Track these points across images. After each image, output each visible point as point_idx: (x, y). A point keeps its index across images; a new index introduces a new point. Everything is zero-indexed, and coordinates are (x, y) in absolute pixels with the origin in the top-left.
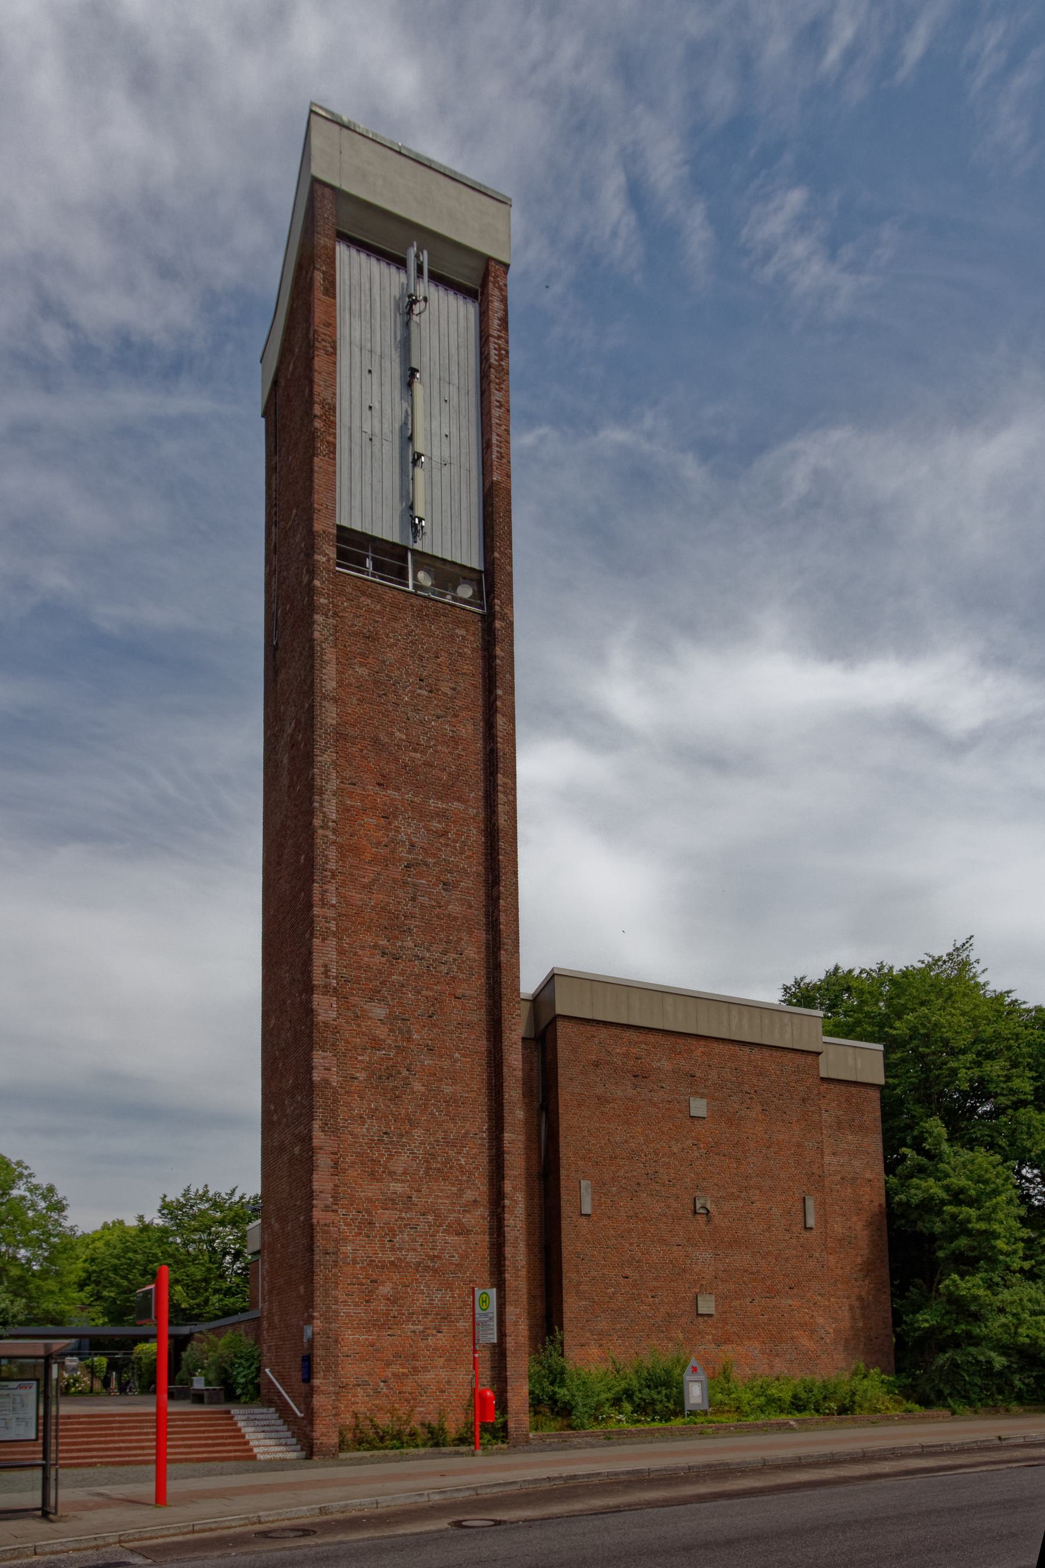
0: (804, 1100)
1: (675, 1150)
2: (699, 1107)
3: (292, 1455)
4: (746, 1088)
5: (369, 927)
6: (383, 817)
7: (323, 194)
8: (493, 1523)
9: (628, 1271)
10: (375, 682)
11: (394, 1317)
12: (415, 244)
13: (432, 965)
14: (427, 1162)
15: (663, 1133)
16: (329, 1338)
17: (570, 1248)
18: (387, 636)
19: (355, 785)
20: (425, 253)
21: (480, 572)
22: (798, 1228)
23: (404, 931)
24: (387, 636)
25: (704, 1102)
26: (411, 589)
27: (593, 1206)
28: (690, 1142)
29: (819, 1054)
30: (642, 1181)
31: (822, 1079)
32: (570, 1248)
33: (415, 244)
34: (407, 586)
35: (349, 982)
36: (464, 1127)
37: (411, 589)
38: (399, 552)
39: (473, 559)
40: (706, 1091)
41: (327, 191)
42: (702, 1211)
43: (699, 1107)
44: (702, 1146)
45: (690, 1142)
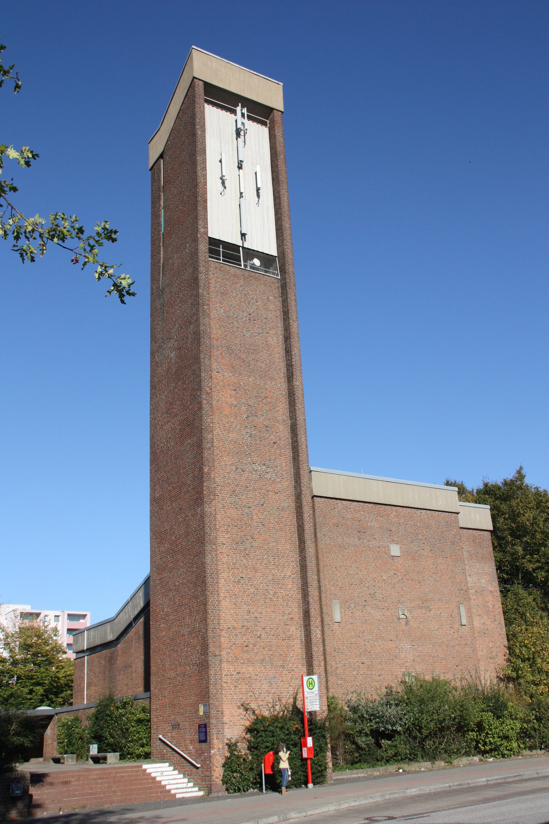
0: (453, 543)
1: (385, 578)
2: (395, 550)
3: (201, 793)
4: (420, 537)
5: (229, 453)
6: (234, 390)
7: (198, 84)
8: (387, 818)
9: (364, 659)
10: (228, 317)
11: (251, 696)
12: (240, 104)
13: (262, 474)
14: (265, 594)
15: (377, 566)
16: (218, 711)
17: (330, 645)
18: (232, 291)
19: (219, 373)
20: (245, 109)
21: (276, 257)
22: (457, 626)
23: (247, 455)
24: (232, 291)
25: (398, 546)
26: (243, 267)
27: (341, 617)
28: (392, 572)
29: (458, 513)
30: (368, 599)
31: (461, 528)
32: (330, 645)
33: (240, 104)
34: (241, 265)
35: (219, 486)
36: (283, 571)
37: (243, 267)
38: (234, 248)
39: (272, 250)
40: (398, 540)
41: (201, 82)
42: (403, 616)
43: (395, 550)
44: (399, 574)
45: (392, 572)
